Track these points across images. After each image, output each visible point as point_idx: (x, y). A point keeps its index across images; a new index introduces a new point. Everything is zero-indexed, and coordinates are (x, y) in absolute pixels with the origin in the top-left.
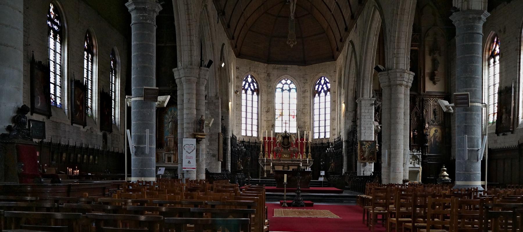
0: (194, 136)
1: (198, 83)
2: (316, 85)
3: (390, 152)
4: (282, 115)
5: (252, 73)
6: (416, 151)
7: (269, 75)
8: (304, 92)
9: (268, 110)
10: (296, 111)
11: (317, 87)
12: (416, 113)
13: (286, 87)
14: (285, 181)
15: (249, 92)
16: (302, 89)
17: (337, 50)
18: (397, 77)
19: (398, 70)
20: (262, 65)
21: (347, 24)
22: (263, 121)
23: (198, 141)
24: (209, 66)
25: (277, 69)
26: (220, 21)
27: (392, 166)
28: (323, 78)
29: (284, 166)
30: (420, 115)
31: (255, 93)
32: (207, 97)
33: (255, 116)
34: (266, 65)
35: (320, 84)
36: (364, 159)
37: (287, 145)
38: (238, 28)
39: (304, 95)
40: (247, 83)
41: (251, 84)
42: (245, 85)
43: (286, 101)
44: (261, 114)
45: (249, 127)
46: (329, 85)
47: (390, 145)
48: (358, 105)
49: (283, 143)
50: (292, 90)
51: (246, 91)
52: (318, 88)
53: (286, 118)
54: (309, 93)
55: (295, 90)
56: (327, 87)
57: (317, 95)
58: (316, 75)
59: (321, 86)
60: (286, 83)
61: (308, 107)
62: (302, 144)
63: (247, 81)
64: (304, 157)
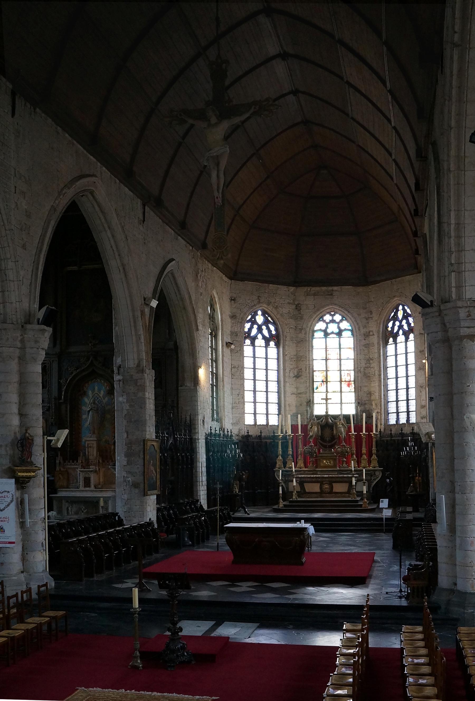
0: (11, 473)
1: (22, 359)
2: (389, 321)
3: (454, 500)
4: (327, 382)
5: (265, 306)
7: (298, 307)
8: (367, 335)
9: (297, 373)
10: (352, 373)
11: (390, 324)
13: (333, 328)
14: (136, 604)
15: (260, 342)
16: (363, 331)
18: (459, 320)
19: (459, 304)
20: (283, 290)
22: (288, 394)
23: (22, 484)
25: (314, 295)
27: (458, 534)
28: (401, 307)
29: (322, 484)
31: (272, 344)
32: (122, 370)
33: (273, 387)
34: (292, 289)
35: (395, 318)
40: (255, 326)
41: (264, 327)
42: (250, 329)
43: (333, 354)
44: (285, 382)
45: (261, 408)
46: (411, 320)
47: (452, 483)
48: (19, 503)
49: (322, 438)
50: (344, 334)
51: (253, 340)
52: (393, 328)
53: (334, 386)
54: (376, 336)
55: (349, 333)
56: (409, 324)
57: (391, 340)
58: (388, 302)
59: (397, 323)
60: (333, 321)
61: (374, 364)
62: (358, 438)
63: (253, 322)
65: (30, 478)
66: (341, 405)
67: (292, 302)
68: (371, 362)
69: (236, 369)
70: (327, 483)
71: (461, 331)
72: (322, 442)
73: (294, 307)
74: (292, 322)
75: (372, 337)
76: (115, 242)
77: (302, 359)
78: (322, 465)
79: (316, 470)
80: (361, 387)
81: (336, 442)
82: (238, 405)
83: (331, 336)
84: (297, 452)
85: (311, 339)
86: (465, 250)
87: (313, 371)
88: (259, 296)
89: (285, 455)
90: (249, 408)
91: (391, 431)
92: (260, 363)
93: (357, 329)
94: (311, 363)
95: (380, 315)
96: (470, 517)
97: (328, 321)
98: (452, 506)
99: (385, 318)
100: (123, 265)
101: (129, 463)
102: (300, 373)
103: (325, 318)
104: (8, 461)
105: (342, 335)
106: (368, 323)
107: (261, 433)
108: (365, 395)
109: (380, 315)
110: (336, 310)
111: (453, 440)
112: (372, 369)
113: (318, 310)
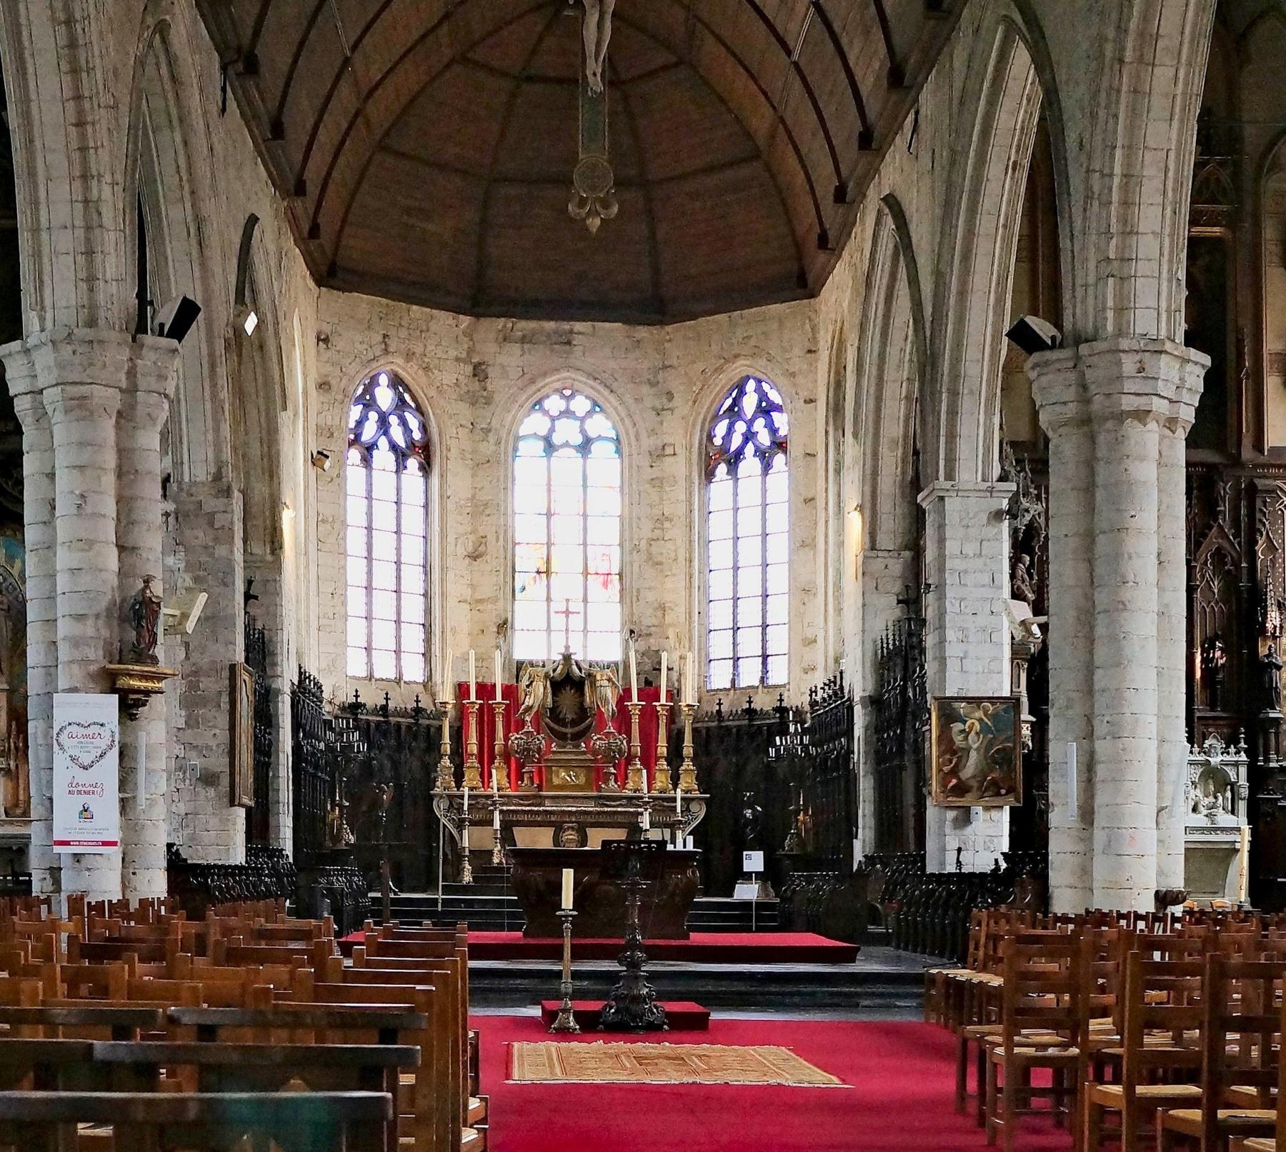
0: (108, 681)
1: (125, 418)
2: (716, 418)
3: (1092, 753)
4: (548, 572)
6: (1220, 745)
7: (479, 372)
8: (659, 454)
9: (481, 545)
10: (616, 553)
12: (1219, 556)
13: (567, 432)
15: (383, 457)
16: (648, 442)
17: (823, 241)
18: (1120, 377)
20: (443, 318)
21: (872, 114)
22: (452, 602)
23: (130, 707)
24: (179, 329)
25: (523, 340)
26: (232, 105)
27: (1100, 820)
28: (751, 386)
29: (559, 828)
30: (1237, 564)
31: (413, 463)
32: (173, 487)
34: (465, 321)
35: (734, 412)
36: (961, 790)
37: (574, 723)
38: (322, 135)
39: (655, 473)
41: (393, 420)
42: (360, 423)
43: (568, 502)
44: (444, 569)
46: (780, 419)
49: (555, 713)
50: (595, 447)
53: (566, 584)
54: (681, 459)
57: (722, 469)
59: (741, 427)
60: (567, 413)
61: (676, 532)
63: (369, 403)
64: (662, 780)
65: (147, 693)
66: (585, 636)
67: (464, 355)
68: (667, 525)
69: (328, 526)
70: (572, 828)
71: (1124, 401)
72: (552, 725)
73: (469, 369)
74: (464, 410)
75: (672, 459)
76: (189, 157)
77: (487, 512)
78: (556, 781)
79: (541, 797)
80: (638, 591)
81: (589, 727)
82: (333, 622)
83: (562, 452)
84: (492, 747)
85: (510, 459)
86: (1137, 233)
87: (514, 544)
88: (385, 336)
89: (458, 754)
90: (356, 632)
91: (720, 704)
92: (384, 516)
93: (633, 438)
94: (510, 522)
95: (695, 402)
96: (1128, 785)
97: (555, 413)
98: (1089, 767)
99: (707, 412)
100: (199, 221)
101: (192, 722)
102: (482, 549)
103: (547, 404)
104: (101, 653)
105: (590, 452)
106: (661, 423)
107: (387, 699)
108: (650, 611)
109: (695, 402)
110: (577, 385)
111: (1092, 628)
112: (669, 545)
113: (532, 381)
